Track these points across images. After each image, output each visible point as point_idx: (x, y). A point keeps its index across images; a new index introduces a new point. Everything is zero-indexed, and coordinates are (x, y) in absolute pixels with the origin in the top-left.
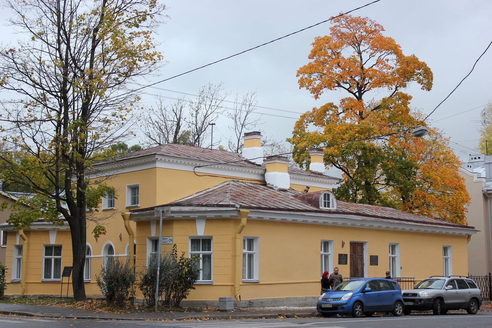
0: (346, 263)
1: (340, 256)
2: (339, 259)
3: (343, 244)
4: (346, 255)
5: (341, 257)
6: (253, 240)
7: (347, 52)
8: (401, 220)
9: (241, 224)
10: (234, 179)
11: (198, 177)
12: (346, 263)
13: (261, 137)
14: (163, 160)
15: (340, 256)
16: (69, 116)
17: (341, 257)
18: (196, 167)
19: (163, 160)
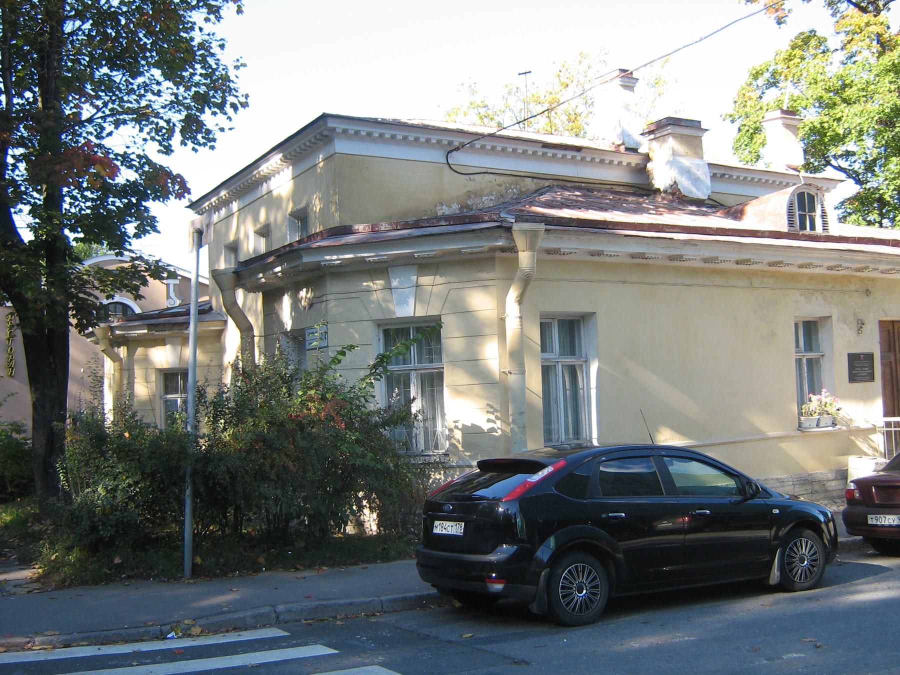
0: (872, 379)
1: (853, 359)
2: (851, 367)
3: (861, 325)
4: (870, 357)
5: (856, 363)
6: (579, 321)
7: (96, 149)
8: (544, 179)
9: (519, 273)
10: (562, 183)
11: (453, 172)
12: (872, 379)
13: (634, 81)
14: (411, 139)
15: (853, 359)
16: (887, 523)
17: (856, 363)
18: (452, 151)
19: (510, 150)
